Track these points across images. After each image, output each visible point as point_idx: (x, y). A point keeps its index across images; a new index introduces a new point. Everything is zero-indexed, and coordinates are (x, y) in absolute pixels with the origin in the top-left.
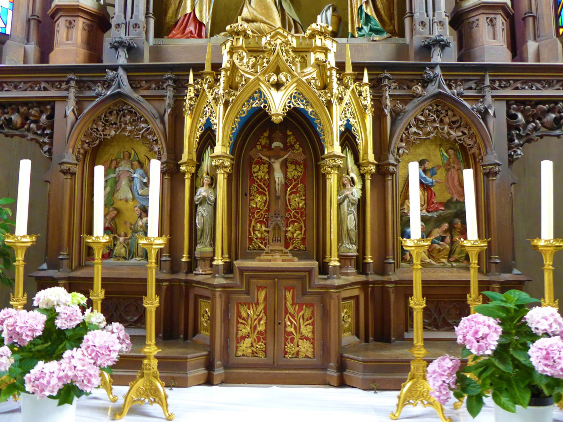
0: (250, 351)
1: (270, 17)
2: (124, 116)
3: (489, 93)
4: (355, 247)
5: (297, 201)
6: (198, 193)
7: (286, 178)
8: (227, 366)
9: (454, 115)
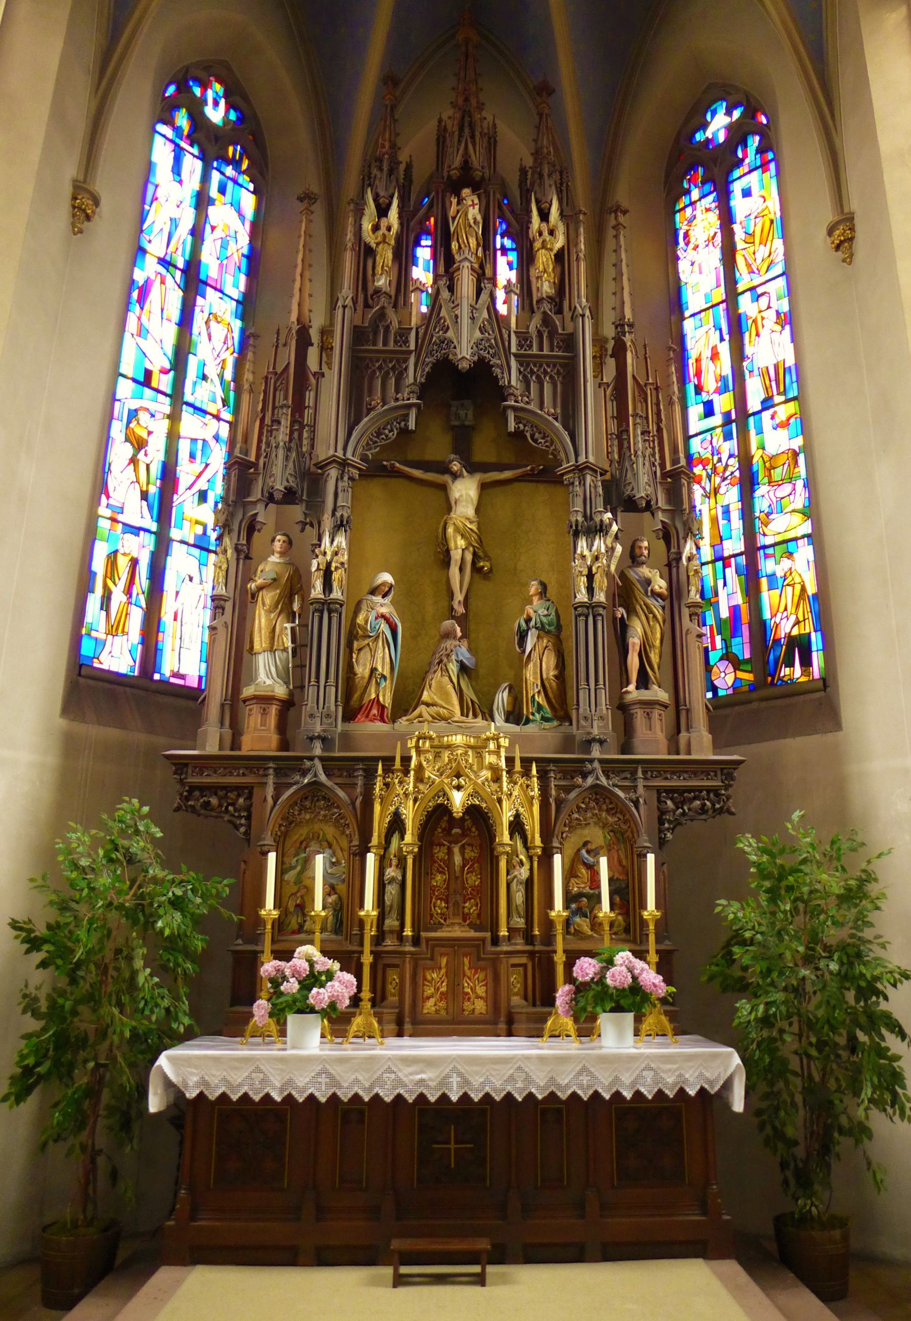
0: (433, 1009)
1: (448, 701)
2: (318, 800)
3: (641, 783)
4: (523, 920)
5: (473, 880)
6: (387, 873)
7: (464, 859)
8: (414, 1022)
9: (611, 803)
